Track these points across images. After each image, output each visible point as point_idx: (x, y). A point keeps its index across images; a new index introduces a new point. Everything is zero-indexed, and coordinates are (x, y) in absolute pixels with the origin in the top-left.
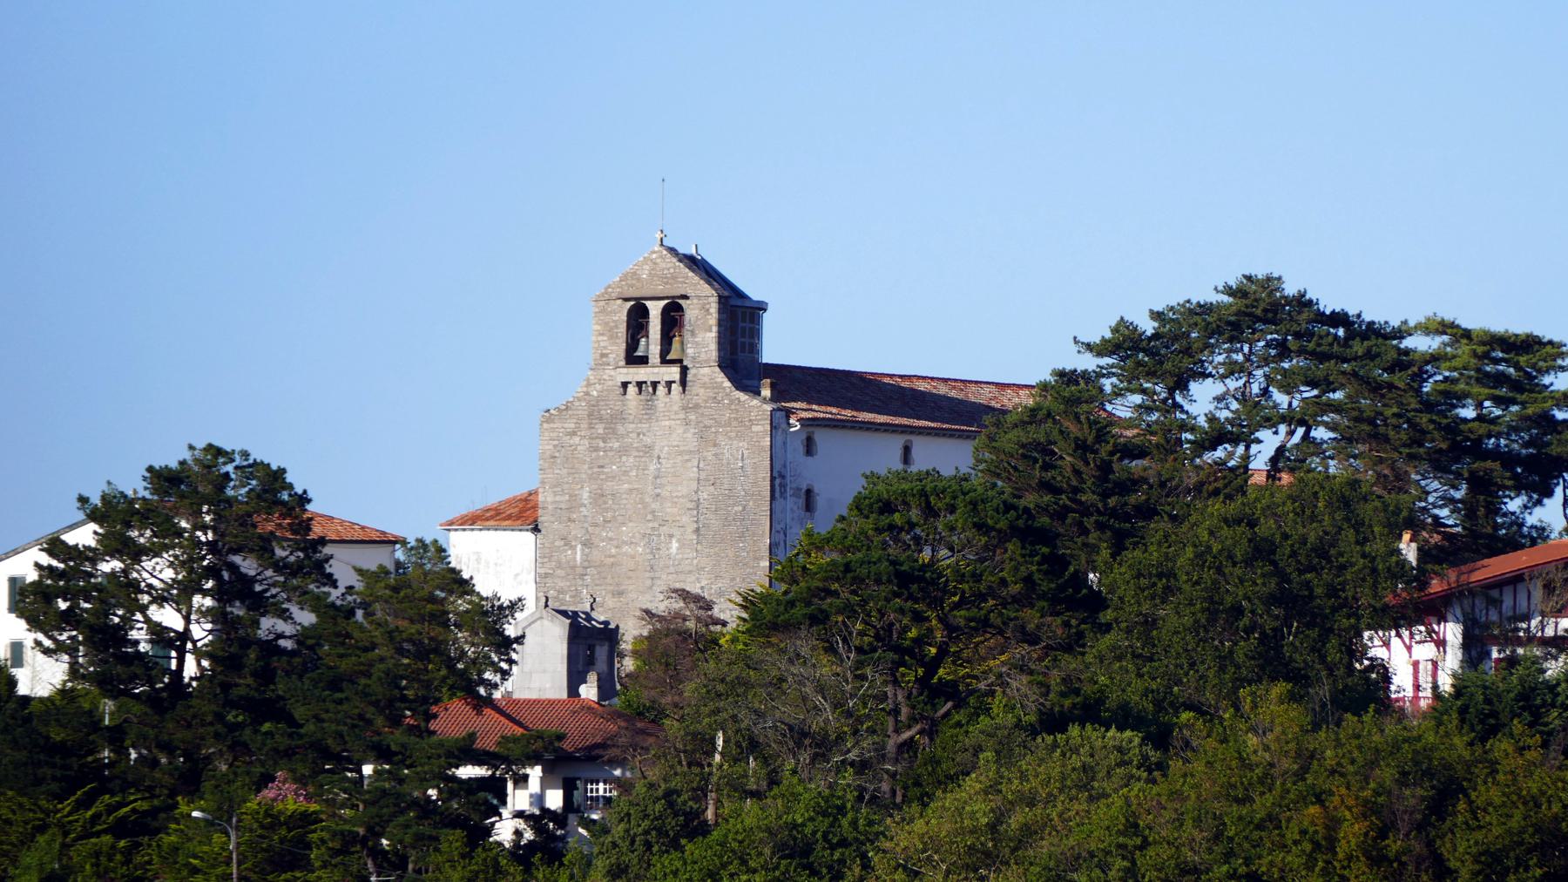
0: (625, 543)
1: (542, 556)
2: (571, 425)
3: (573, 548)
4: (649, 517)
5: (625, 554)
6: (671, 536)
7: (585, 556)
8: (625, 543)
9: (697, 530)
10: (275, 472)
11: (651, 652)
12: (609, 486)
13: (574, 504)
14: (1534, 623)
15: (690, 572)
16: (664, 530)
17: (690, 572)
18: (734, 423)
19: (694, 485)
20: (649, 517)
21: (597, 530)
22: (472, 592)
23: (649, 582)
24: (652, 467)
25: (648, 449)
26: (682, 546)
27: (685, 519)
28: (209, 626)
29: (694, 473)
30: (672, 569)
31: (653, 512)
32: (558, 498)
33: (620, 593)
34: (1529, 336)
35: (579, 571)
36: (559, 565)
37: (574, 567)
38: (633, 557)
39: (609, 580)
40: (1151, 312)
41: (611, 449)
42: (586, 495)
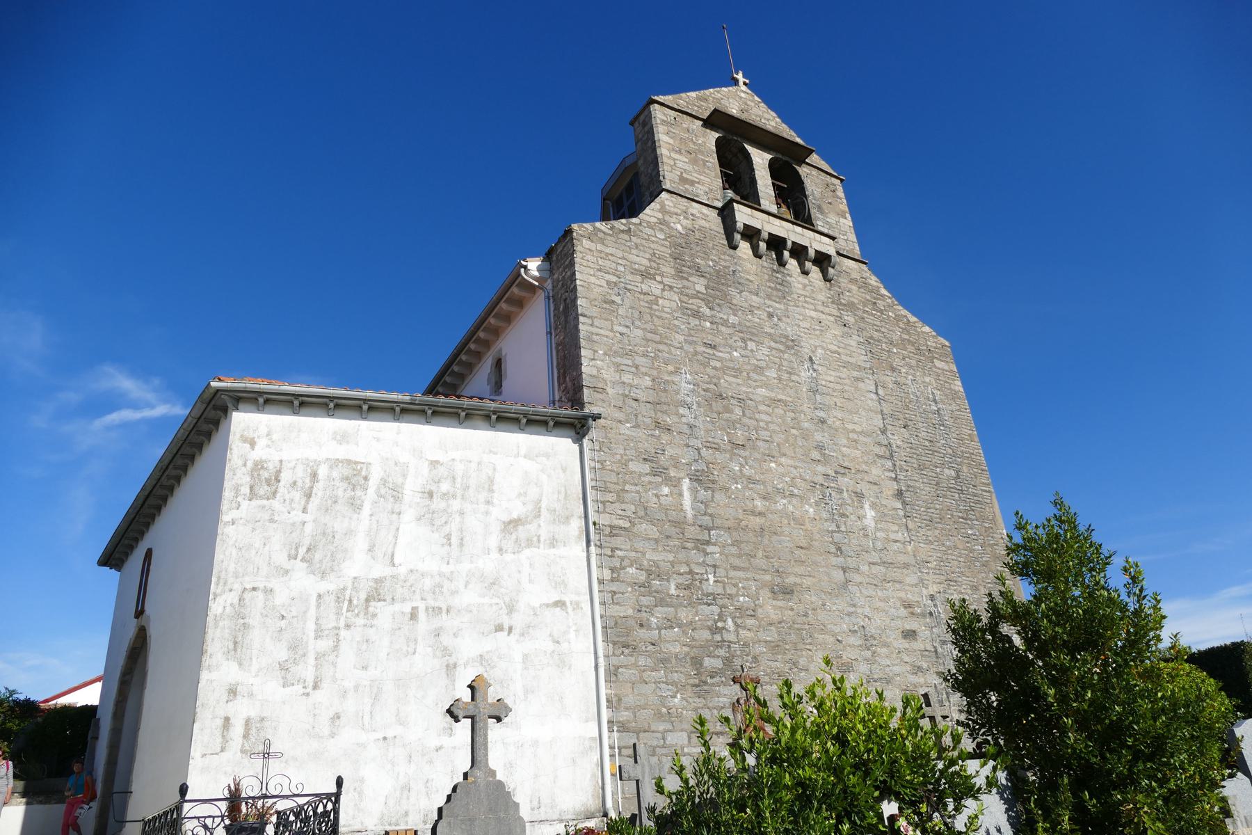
1: (598, 490)
2: (642, 261)
3: (675, 483)
4: (815, 455)
5: (784, 513)
6: (860, 496)
7: (703, 507)
8: (782, 493)
9: (899, 494)
11: (968, 674)
12: (729, 383)
13: (662, 399)
15: (906, 566)
16: (844, 481)
17: (906, 566)
21: (721, 458)
23: (838, 576)
25: (791, 344)
27: (876, 471)
28: (251, 820)
30: (875, 557)
31: (820, 447)
34: (1233, 644)
35: (692, 532)
36: (646, 514)
37: (679, 524)
39: (760, 561)
41: (725, 323)
42: (685, 387)
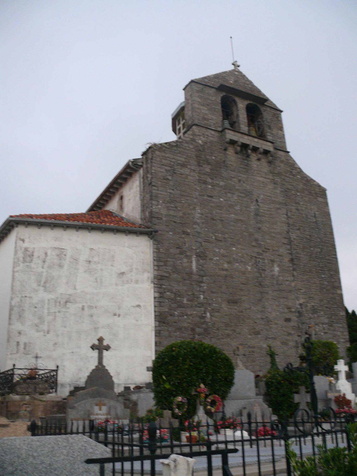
0: (236, 261)
2: (182, 159)
3: (189, 257)
6: (273, 261)
7: (201, 268)
8: (236, 261)
10: (332, 369)
14: (199, 211)
15: (290, 291)
18: (306, 192)
19: (285, 228)
20: (254, 244)
22: (337, 382)
24: (253, 207)
25: (248, 194)
26: (282, 270)
29: (283, 218)
31: (256, 240)
32: (171, 213)
33: (235, 302)
35: (195, 277)
38: (244, 273)
40: (232, 117)
41: (218, 185)
42: (198, 215)
